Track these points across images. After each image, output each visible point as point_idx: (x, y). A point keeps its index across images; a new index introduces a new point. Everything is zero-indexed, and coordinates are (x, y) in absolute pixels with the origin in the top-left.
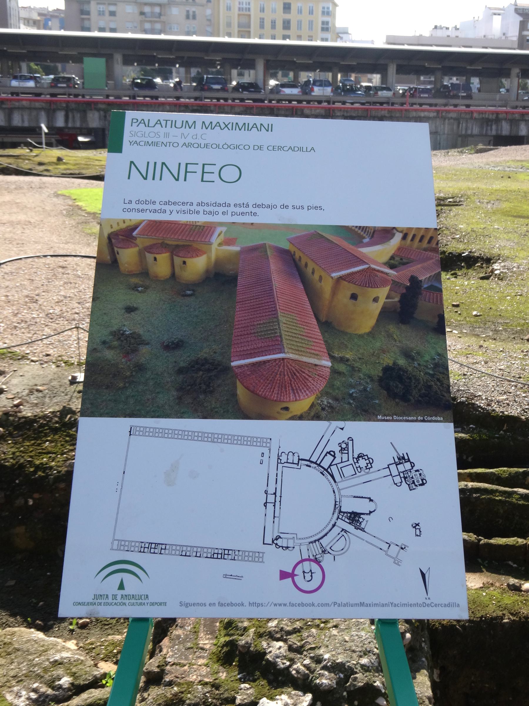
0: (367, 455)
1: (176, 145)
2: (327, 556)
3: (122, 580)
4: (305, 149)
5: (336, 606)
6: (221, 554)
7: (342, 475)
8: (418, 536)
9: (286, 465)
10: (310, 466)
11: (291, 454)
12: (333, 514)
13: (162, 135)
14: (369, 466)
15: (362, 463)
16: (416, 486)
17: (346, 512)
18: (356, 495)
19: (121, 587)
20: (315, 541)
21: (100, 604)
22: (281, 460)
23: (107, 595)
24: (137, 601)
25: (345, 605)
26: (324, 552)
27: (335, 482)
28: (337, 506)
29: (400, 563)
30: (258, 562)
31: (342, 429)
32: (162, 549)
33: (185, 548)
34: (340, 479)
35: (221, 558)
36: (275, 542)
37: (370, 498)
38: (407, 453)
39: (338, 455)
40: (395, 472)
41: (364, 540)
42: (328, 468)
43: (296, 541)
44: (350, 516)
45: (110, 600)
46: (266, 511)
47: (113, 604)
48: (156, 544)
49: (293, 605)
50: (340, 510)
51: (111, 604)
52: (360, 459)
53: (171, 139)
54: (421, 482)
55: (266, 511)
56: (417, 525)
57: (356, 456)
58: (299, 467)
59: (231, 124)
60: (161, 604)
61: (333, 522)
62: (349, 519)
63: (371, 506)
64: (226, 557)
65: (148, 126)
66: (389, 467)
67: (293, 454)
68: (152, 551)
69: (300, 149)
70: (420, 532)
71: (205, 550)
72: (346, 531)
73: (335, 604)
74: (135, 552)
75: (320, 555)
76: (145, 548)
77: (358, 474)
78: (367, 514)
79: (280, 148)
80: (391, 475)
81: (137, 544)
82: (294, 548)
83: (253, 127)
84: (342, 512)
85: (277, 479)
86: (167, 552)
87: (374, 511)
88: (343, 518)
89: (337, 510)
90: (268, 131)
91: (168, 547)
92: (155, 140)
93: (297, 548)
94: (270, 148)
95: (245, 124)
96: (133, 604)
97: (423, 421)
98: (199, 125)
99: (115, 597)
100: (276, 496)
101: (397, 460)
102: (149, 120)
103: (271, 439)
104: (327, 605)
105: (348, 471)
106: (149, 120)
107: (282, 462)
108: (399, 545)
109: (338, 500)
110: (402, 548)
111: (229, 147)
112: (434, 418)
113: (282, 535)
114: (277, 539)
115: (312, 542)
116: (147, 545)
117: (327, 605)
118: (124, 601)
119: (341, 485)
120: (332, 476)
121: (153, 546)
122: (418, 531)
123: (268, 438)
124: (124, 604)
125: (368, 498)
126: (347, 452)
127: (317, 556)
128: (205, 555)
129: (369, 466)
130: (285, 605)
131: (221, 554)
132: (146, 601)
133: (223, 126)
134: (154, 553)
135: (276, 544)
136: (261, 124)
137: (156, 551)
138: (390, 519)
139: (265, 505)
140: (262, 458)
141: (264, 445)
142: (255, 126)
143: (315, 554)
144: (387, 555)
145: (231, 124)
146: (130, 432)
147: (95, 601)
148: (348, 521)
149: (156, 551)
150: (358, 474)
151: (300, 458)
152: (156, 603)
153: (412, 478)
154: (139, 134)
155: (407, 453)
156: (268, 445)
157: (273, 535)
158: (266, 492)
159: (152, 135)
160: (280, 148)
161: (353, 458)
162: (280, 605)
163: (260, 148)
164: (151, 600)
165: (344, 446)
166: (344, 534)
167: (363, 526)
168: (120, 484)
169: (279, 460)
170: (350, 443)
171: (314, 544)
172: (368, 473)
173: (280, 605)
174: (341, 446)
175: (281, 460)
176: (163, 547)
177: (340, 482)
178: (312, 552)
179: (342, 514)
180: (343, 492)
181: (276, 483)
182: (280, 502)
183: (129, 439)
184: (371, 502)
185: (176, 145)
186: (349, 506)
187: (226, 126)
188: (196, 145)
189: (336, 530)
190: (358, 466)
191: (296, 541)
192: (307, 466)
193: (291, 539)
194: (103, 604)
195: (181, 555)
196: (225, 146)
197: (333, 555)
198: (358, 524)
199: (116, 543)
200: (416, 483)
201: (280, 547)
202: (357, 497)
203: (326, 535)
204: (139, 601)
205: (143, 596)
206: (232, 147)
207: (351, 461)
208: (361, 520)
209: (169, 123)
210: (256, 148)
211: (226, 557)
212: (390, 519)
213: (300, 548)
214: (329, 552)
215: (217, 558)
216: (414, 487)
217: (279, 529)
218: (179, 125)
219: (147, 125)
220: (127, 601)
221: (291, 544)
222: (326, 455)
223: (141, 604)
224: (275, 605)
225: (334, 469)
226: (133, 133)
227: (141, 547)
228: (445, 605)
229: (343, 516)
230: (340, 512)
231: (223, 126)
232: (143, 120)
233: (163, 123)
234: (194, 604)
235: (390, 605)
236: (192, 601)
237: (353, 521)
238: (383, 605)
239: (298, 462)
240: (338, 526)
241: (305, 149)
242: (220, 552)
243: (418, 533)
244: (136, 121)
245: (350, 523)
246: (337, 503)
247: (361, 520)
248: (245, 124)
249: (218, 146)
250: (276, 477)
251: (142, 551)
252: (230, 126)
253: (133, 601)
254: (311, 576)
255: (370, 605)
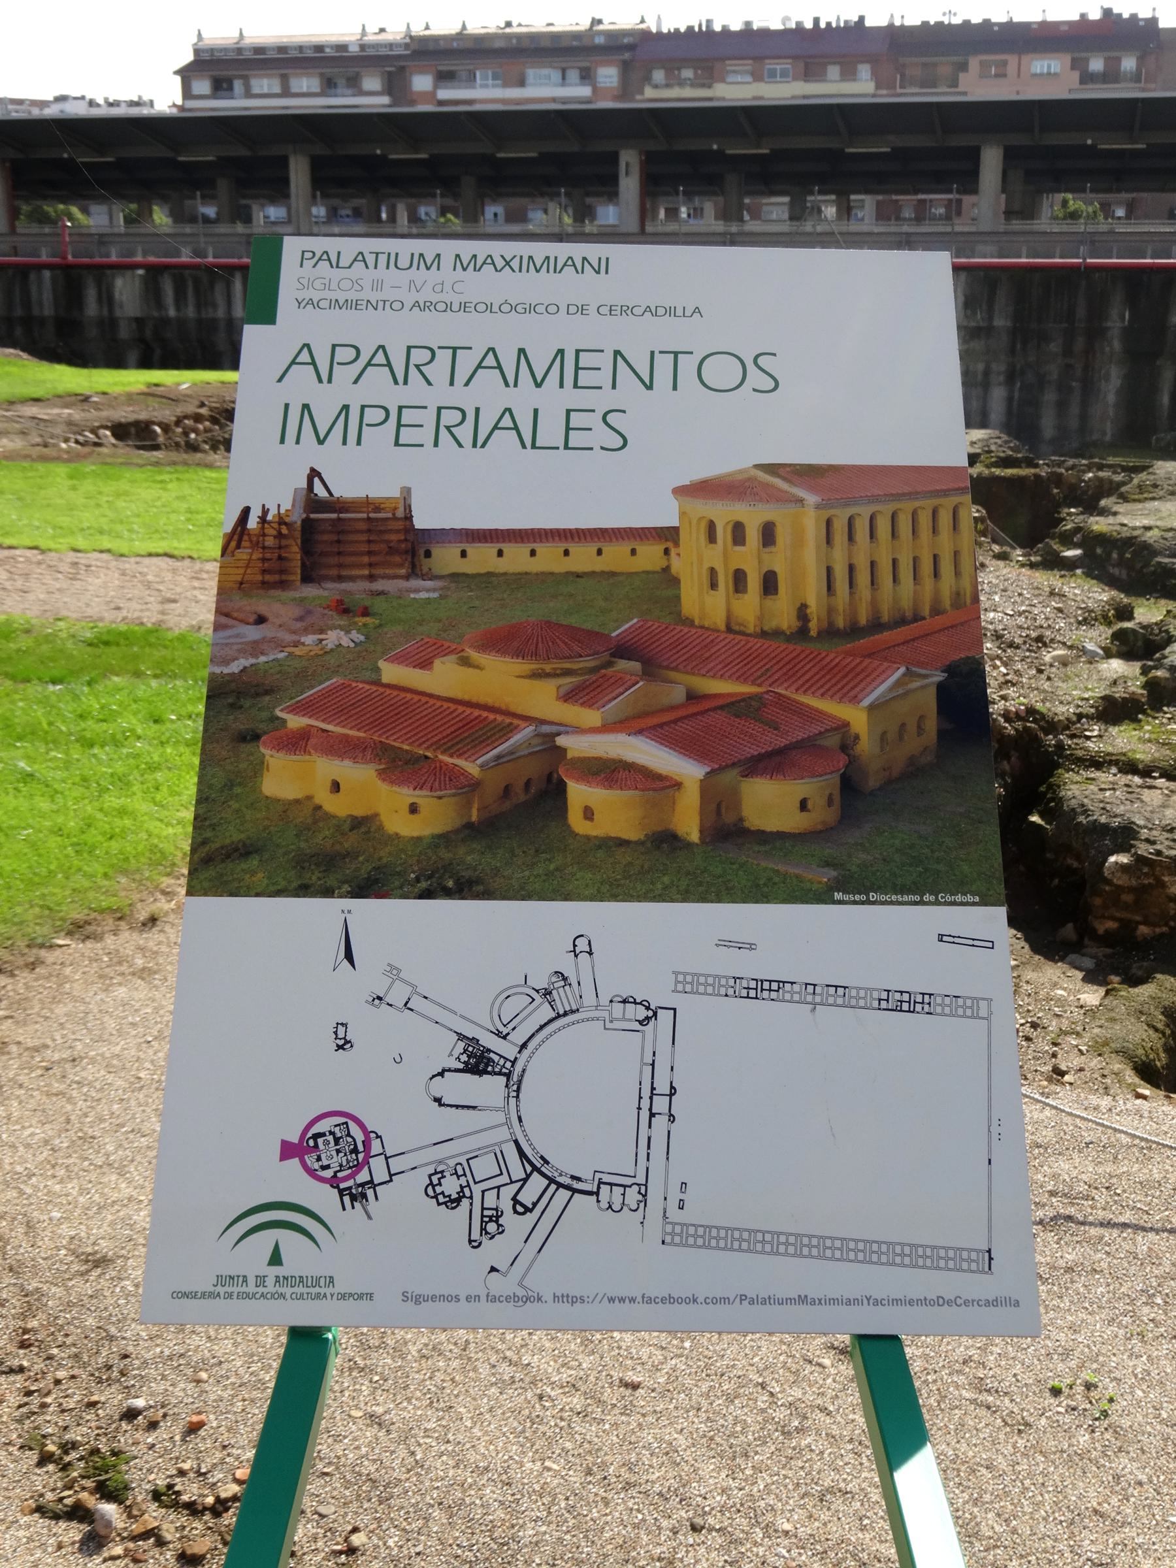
0: (439, 1204)
1: (397, 306)
2: (542, 984)
3: (277, 1246)
4: (679, 312)
5: (745, 1303)
6: (762, 989)
7: (500, 1159)
8: (342, 1024)
9: (628, 1181)
10: (573, 1177)
11: (616, 1207)
12: (524, 1071)
13: (367, 285)
14: (435, 1180)
15: (450, 1186)
16: (331, 1133)
17: (496, 1074)
18: (471, 1112)
19: (276, 1259)
20: (566, 1014)
21: (230, 1295)
22: (639, 1193)
23: (245, 1277)
24: (309, 1290)
25: (764, 1302)
26: (548, 993)
27: (516, 1142)
28: (515, 1087)
29: (388, 969)
30: (685, 974)
31: (493, 1269)
32: (887, 1000)
33: (840, 1001)
34: (504, 1147)
35: (762, 981)
36: (650, 1013)
37: (441, 1105)
38: (344, 1209)
39: (506, 1205)
40: (378, 1164)
41: (461, 1016)
42: (531, 1173)
43: (606, 1014)
44: (487, 1065)
45: (251, 1288)
46: (672, 1076)
47: (258, 1296)
48: (901, 1011)
49: (650, 1301)
50: (508, 1080)
51: (254, 1295)
52: (454, 1196)
53: (388, 294)
54: (320, 1141)
55: (672, 1076)
56: (340, 1047)
57: (465, 1203)
58: (598, 1176)
59: (518, 259)
60: (360, 1296)
61: (526, 1053)
62: (490, 1060)
63: (440, 1087)
64: (753, 984)
65: (337, 267)
66: (391, 1175)
67: (610, 1207)
68: (906, 997)
69: (671, 312)
70: (336, 1033)
71: (796, 997)
72: (498, 1034)
73: (743, 1298)
74: (939, 995)
75: (556, 985)
76: (923, 1003)
77: (463, 1160)
78: (449, 1070)
79: (627, 310)
80: (387, 1158)
81: (939, 1009)
82: (611, 1001)
83: (565, 265)
84: (504, 1074)
85: (649, 1147)
86: (876, 995)
87: (434, 1076)
88: (502, 1062)
89: (515, 1079)
90: (598, 272)
91: (875, 1004)
92: (352, 296)
93: (604, 1000)
94: (604, 310)
95: (548, 258)
96: (301, 1297)
97: (937, 903)
98: (447, 261)
99: (261, 1280)
100: (650, 1109)
101: (370, 1193)
102: (339, 253)
103: (663, 1242)
104: (725, 1300)
105: (484, 1167)
106: (339, 253)
107: (636, 1188)
108: (384, 1006)
109: (513, 1101)
110: (380, 998)
111: (513, 308)
112: (959, 898)
113: (637, 1026)
114: (648, 1018)
115: (573, 1012)
116: (918, 1007)
117: (725, 1300)
118: (281, 1290)
119: (504, 1134)
120: (522, 1154)
121: (905, 1006)
122: (341, 1034)
123: (669, 1244)
124: (282, 1296)
125: (444, 1105)
126: (486, 1213)
127: (562, 983)
128: (796, 988)
129: (435, 1180)
130: (632, 1300)
131: (762, 990)
132: (328, 1291)
133: (500, 263)
134: (902, 992)
135: (648, 1008)
136: (584, 259)
137: (898, 996)
138: (398, 1060)
139: (673, 1091)
140: (682, 1196)
141: (678, 1229)
142: (570, 262)
143: (567, 988)
144: (414, 987)
145: (517, 260)
146: (991, 1259)
147: (219, 1289)
148: (492, 1055)
149: (898, 996)
150: (463, 1160)
151: (595, 1197)
152: (351, 1295)
153: (338, 1151)
154: (317, 284)
155: (344, 1209)
156: (669, 1228)
157: (655, 1029)
158: (672, 1118)
159: (346, 284)
160: (627, 310)
161: (471, 1197)
162: (622, 1300)
163: (582, 309)
164: (340, 1287)
165: (492, 1227)
166: (501, 1028)
167: (461, 1045)
168: (995, 1136)
169: (643, 1191)
170: (476, 1235)
171: (568, 1008)
172: (440, 1162)
173: (622, 1300)
174: (499, 1226)
175: (639, 1193)
176: (884, 1004)
177: (506, 1141)
178: (573, 992)
179: (504, 1070)
180: (500, 1117)
181: (649, 1138)
182: (640, 1098)
183: (990, 1241)
184: (438, 1096)
185: (397, 306)
186: (490, 1088)
187: (508, 263)
188: (441, 307)
189: (519, 1037)
190: (463, 1179)
191: (606, 1014)
192: (578, 1179)
193: (617, 1019)
194: (235, 1296)
195: (845, 988)
196: (506, 308)
197: (529, 987)
198: (470, 1049)
199: (983, 1013)
200: (331, 1138)
201: (640, 1003)
202: (468, 1107)
203: (542, 1027)
204: (314, 1290)
205: (322, 1280)
206: (519, 309)
207: (477, 1190)
208: (464, 1058)
209: (383, 259)
210: (573, 309)
211: (753, 984)
212: (398, 1060)
213: (598, 1001)
214: (537, 991)
215: (771, 981)
216: (337, 1130)
217: (644, 1037)
218: (404, 262)
219: (334, 264)
220: (288, 1291)
221: (618, 1008)
222: (535, 1204)
223: (318, 1296)
224: (611, 1300)
225: (518, 1172)
226: (304, 281)
227: (929, 1004)
228: (988, 1303)
229: (503, 1066)
230: (508, 1076)
231: (500, 263)
232: (326, 252)
233: (371, 259)
234: (433, 1298)
235: (865, 1301)
236: (427, 1291)
237: (482, 1056)
238: (849, 1302)
239: (599, 1188)
240: (516, 1045)
241: (679, 312)
242: (766, 994)
243: (341, 1030)
244: (311, 255)
245: (489, 1051)
246: (515, 1094)
247: (464, 1058)
248: (548, 258)
249: (489, 308)
250: (651, 1152)
251: (926, 997)
252: (515, 264)
253: (300, 1290)
254: (575, 946)
255: (820, 1300)
